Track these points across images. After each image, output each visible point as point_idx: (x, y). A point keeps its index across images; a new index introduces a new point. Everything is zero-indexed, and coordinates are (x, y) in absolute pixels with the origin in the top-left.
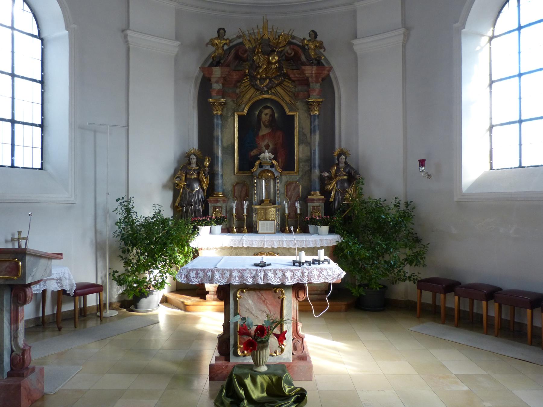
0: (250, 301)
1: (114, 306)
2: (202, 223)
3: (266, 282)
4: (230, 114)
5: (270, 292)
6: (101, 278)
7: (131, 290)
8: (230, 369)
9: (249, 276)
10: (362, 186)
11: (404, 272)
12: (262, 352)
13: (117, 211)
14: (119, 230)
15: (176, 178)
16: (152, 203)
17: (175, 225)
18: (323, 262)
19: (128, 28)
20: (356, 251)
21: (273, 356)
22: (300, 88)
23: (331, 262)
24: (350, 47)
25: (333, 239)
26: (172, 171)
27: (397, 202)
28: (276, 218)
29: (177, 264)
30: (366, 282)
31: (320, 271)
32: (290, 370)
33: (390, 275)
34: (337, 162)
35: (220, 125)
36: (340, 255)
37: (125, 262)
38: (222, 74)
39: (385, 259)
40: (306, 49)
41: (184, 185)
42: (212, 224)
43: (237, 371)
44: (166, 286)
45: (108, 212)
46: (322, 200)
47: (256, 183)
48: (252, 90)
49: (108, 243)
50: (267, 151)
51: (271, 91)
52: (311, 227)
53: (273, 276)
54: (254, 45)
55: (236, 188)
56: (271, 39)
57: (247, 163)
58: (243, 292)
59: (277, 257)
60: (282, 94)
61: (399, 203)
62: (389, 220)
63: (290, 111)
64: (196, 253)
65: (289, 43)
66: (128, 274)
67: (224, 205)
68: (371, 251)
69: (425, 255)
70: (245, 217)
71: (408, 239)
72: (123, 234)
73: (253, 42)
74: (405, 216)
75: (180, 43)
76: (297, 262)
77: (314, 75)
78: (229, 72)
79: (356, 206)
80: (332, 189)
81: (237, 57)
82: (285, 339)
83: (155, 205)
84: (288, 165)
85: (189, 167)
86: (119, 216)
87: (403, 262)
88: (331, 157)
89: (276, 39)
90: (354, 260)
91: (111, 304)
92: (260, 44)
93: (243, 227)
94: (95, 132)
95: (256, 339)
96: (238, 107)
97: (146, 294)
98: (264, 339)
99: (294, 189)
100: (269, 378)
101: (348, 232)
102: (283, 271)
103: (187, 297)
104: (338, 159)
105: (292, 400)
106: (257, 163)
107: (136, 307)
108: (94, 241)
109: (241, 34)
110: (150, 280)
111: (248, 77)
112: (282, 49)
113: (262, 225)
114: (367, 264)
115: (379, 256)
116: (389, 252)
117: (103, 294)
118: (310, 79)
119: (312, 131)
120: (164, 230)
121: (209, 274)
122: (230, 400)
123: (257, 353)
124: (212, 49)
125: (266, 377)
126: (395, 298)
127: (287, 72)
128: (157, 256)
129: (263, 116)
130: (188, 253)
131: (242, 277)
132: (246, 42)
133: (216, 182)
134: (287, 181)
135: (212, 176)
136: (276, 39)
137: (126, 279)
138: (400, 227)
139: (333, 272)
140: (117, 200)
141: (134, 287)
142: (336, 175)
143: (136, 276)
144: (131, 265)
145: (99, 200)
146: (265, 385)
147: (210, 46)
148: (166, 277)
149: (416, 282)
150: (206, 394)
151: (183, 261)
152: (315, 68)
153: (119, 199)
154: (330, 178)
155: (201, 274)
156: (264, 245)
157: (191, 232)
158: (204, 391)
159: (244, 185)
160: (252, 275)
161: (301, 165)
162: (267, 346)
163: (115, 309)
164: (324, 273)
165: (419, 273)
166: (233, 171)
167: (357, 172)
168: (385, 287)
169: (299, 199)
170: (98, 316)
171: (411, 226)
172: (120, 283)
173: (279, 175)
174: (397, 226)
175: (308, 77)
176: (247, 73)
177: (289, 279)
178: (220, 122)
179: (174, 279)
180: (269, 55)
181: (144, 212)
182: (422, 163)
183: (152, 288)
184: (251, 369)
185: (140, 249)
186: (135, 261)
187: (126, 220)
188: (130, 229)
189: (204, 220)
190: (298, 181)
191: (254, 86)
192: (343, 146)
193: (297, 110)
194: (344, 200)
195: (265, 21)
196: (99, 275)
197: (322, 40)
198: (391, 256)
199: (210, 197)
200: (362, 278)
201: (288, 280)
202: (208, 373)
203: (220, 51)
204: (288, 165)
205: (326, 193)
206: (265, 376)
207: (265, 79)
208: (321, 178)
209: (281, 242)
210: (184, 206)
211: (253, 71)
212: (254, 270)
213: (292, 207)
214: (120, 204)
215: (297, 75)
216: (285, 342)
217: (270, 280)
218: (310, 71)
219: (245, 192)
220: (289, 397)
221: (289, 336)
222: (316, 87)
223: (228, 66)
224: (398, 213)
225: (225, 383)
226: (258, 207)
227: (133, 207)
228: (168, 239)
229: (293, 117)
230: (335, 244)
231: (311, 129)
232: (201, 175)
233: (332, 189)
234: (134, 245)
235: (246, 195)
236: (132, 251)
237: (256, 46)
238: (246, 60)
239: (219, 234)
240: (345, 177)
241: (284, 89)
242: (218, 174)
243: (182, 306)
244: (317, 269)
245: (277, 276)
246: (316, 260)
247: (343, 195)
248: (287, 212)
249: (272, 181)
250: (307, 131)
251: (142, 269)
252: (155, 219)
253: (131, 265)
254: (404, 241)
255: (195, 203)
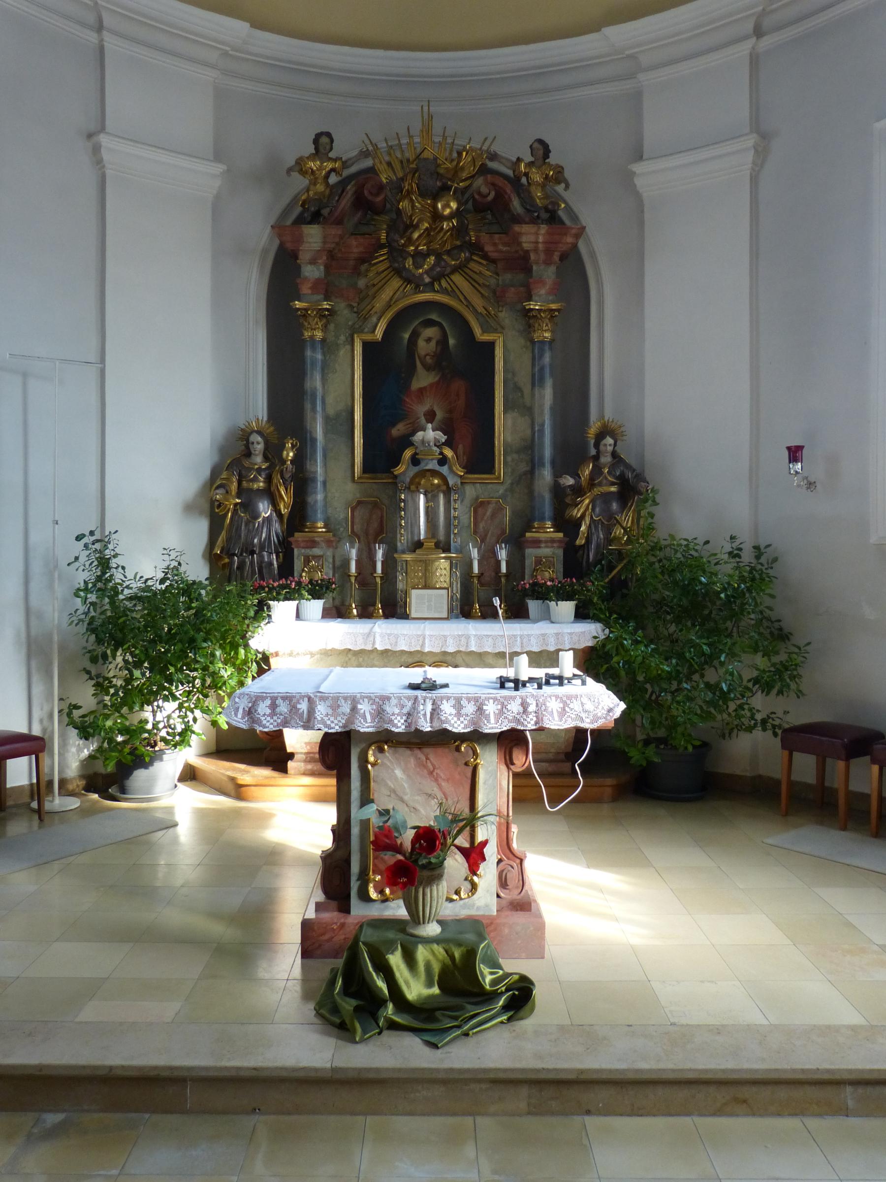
0: (398, 773)
1: (70, 787)
2: (278, 594)
3: (437, 726)
4: (342, 338)
5: (447, 750)
6: (41, 721)
7: (111, 750)
8: (350, 931)
9: (397, 711)
10: (653, 509)
11: (750, 710)
12: (428, 891)
13: (77, 564)
14: (82, 609)
15: (217, 488)
16: (161, 546)
17: (215, 597)
18: (569, 680)
19: (102, 129)
20: (640, 659)
21: (451, 900)
22: (508, 277)
23: (589, 680)
24: (627, 180)
25: (589, 632)
26: (206, 473)
27: (734, 545)
28: (451, 584)
29: (220, 688)
30: (661, 733)
31: (565, 702)
32: (492, 934)
33: (719, 717)
34: (593, 452)
35: (319, 364)
36: (603, 670)
37: (98, 685)
38: (324, 243)
39: (705, 679)
40: (522, 185)
41: (236, 505)
42: (301, 597)
43: (368, 935)
44: (194, 740)
45: (56, 567)
46: (560, 541)
47: (404, 501)
48: (396, 283)
49: (56, 638)
50: (430, 426)
51: (440, 285)
52: (533, 605)
53: (454, 712)
54: (400, 174)
55: (356, 513)
56: (442, 157)
57: (384, 454)
58: (381, 750)
59: (462, 671)
60: (465, 293)
61: (740, 549)
62: (718, 587)
63: (484, 332)
64: (264, 663)
65: (484, 170)
66: (102, 711)
67: (329, 553)
68: (674, 661)
69: (801, 671)
70: (378, 580)
71: (760, 634)
72: (93, 617)
73: (397, 166)
74: (753, 579)
75: (225, 167)
76: (509, 680)
77: (540, 246)
78: (341, 237)
79: (638, 555)
80: (583, 516)
81: (361, 203)
82: (484, 859)
83: (167, 551)
84: (480, 460)
85: (246, 463)
86: (82, 576)
87: (750, 685)
88: (573, 451)
89: (452, 160)
90: (634, 680)
91: (63, 782)
92: (416, 171)
93: (374, 605)
94: (25, 375)
95: (414, 862)
96: (363, 318)
97: (147, 759)
98: (433, 860)
99: (493, 516)
100: (447, 952)
101: (620, 617)
102: (476, 700)
103: (242, 766)
104: (597, 445)
105: (501, 1003)
106: (408, 454)
107: (123, 791)
108: (23, 635)
109: (371, 148)
110: (155, 726)
111: (385, 251)
112: (467, 183)
113: (418, 601)
114: (665, 690)
115: (692, 672)
116: (716, 662)
117: (45, 758)
118: (533, 256)
119: (537, 380)
120: (189, 608)
121: (303, 706)
122: (354, 1002)
123: (417, 892)
124: (300, 182)
125: (439, 950)
126: (727, 772)
127: (477, 237)
128: (172, 670)
129: (421, 343)
130: (245, 662)
131: (380, 713)
132: (381, 167)
133: (310, 499)
134: (477, 498)
135: (302, 484)
136: (452, 160)
137: (100, 723)
138: (743, 604)
139: (596, 705)
140: (79, 538)
141: (119, 743)
142: (592, 483)
143: (122, 716)
144: (112, 691)
145: (34, 538)
146: (436, 968)
147: (295, 175)
148: (195, 720)
149: (779, 732)
150: (296, 988)
151: (233, 682)
152: (544, 229)
153: (83, 536)
154: (578, 491)
155: (283, 708)
156: (423, 645)
157: (252, 613)
158: (289, 983)
159: (376, 505)
160: (405, 711)
161: (509, 459)
162: (439, 877)
163: (72, 794)
164: (576, 705)
165: (786, 713)
166: (349, 474)
167: (640, 477)
168: (705, 745)
169: (503, 539)
170: (33, 810)
171: (768, 601)
172: (85, 732)
173: (459, 482)
174: (734, 603)
175: (527, 252)
176: (383, 241)
177: (492, 720)
178: (319, 356)
179: (214, 723)
180: (436, 197)
181: (142, 565)
182: (795, 453)
183: (161, 745)
184: (403, 931)
185: (132, 654)
186: (120, 683)
187: (99, 585)
188: (107, 607)
189: (283, 587)
190: (504, 497)
191: (399, 272)
192: (608, 415)
193: (499, 328)
194: (609, 541)
195: (426, 116)
196: (37, 714)
197: (561, 164)
198: (721, 671)
199: (297, 534)
200: (652, 722)
201: (489, 721)
202: (298, 939)
203: (320, 188)
204: (480, 460)
205: (567, 526)
206: (435, 946)
207: (425, 255)
208: (558, 491)
209: (463, 639)
210: (234, 554)
211: (397, 237)
212: (408, 698)
213: (489, 557)
214: (86, 546)
215: (501, 247)
216: (483, 868)
217: (447, 721)
218: (532, 236)
219: (378, 521)
220: (493, 996)
221: (491, 852)
222: (546, 274)
223: (339, 222)
224: (737, 572)
225: (339, 963)
226: (408, 557)
227: (115, 556)
228: (199, 630)
229: (491, 345)
230: (590, 644)
231: (533, 376)
232: (275, 481)
233: (583, 516)
234: (118, 644)
235: (380, 530)
236: (114, 658)
237: (406, 175)
238: (377, 211)
239: (319, 620)
240: (613, 489)
241: (470, 279)
242: (314, 480)
243: (230, 787)
244: (557, 697)
245: (463, 712)
246: (554, 677)
247: (608, 530)
248: (476, 569)
249: (441, 496)
250: (524, 378)
251: (137, 700)
252: (168, 583)
253: (112, 691)
254: (751, 638)
255: (262, 548)
